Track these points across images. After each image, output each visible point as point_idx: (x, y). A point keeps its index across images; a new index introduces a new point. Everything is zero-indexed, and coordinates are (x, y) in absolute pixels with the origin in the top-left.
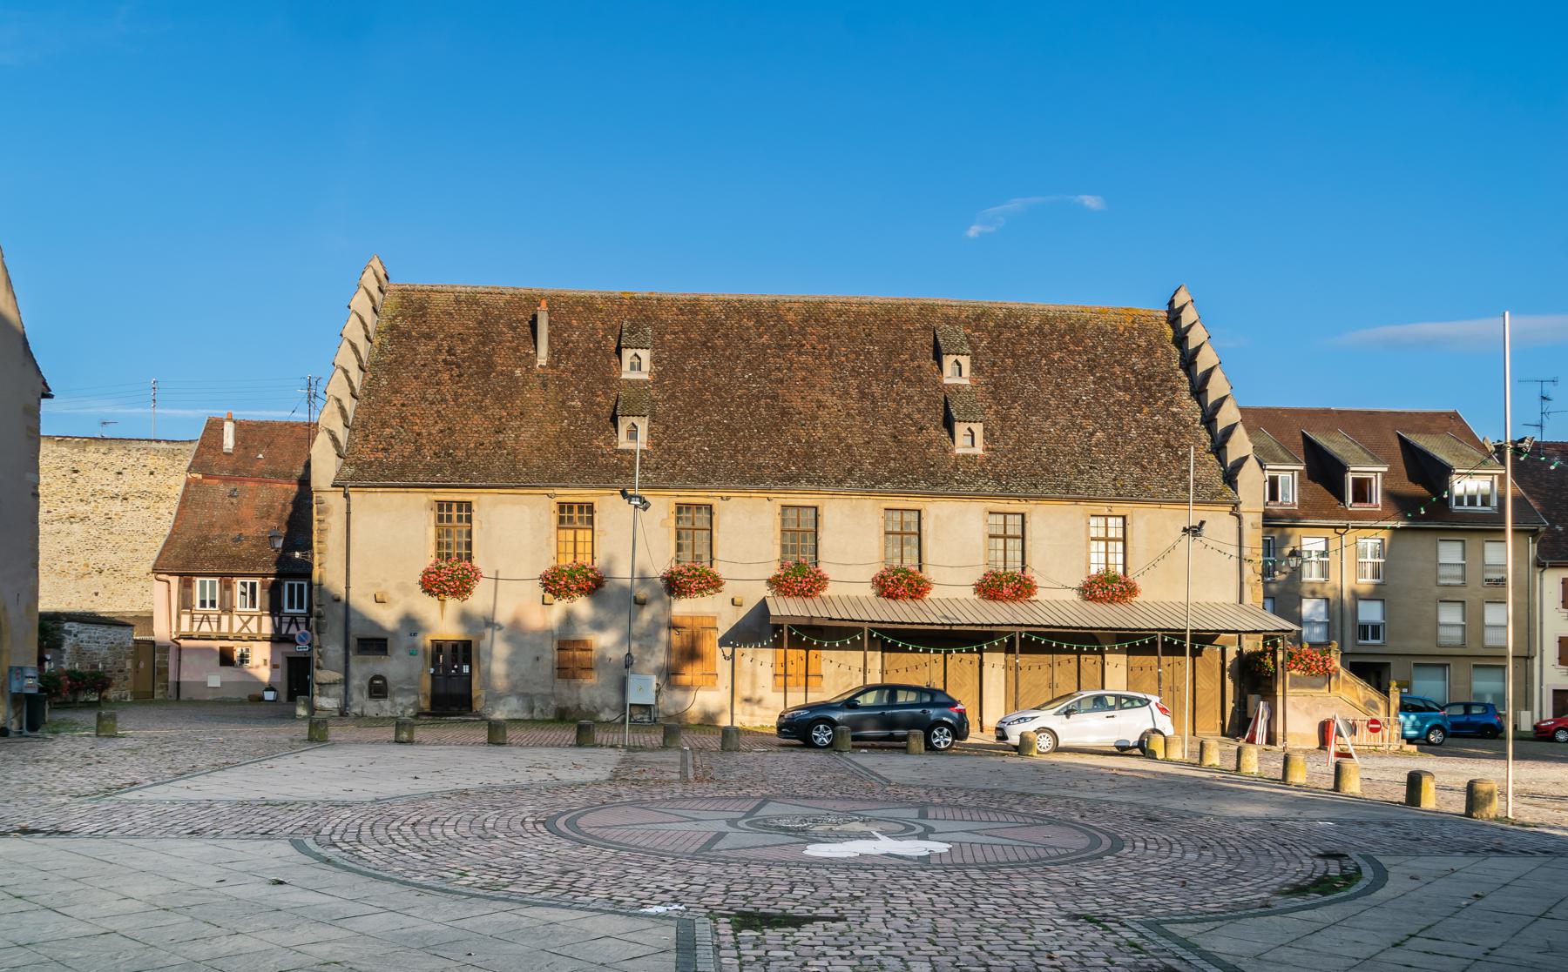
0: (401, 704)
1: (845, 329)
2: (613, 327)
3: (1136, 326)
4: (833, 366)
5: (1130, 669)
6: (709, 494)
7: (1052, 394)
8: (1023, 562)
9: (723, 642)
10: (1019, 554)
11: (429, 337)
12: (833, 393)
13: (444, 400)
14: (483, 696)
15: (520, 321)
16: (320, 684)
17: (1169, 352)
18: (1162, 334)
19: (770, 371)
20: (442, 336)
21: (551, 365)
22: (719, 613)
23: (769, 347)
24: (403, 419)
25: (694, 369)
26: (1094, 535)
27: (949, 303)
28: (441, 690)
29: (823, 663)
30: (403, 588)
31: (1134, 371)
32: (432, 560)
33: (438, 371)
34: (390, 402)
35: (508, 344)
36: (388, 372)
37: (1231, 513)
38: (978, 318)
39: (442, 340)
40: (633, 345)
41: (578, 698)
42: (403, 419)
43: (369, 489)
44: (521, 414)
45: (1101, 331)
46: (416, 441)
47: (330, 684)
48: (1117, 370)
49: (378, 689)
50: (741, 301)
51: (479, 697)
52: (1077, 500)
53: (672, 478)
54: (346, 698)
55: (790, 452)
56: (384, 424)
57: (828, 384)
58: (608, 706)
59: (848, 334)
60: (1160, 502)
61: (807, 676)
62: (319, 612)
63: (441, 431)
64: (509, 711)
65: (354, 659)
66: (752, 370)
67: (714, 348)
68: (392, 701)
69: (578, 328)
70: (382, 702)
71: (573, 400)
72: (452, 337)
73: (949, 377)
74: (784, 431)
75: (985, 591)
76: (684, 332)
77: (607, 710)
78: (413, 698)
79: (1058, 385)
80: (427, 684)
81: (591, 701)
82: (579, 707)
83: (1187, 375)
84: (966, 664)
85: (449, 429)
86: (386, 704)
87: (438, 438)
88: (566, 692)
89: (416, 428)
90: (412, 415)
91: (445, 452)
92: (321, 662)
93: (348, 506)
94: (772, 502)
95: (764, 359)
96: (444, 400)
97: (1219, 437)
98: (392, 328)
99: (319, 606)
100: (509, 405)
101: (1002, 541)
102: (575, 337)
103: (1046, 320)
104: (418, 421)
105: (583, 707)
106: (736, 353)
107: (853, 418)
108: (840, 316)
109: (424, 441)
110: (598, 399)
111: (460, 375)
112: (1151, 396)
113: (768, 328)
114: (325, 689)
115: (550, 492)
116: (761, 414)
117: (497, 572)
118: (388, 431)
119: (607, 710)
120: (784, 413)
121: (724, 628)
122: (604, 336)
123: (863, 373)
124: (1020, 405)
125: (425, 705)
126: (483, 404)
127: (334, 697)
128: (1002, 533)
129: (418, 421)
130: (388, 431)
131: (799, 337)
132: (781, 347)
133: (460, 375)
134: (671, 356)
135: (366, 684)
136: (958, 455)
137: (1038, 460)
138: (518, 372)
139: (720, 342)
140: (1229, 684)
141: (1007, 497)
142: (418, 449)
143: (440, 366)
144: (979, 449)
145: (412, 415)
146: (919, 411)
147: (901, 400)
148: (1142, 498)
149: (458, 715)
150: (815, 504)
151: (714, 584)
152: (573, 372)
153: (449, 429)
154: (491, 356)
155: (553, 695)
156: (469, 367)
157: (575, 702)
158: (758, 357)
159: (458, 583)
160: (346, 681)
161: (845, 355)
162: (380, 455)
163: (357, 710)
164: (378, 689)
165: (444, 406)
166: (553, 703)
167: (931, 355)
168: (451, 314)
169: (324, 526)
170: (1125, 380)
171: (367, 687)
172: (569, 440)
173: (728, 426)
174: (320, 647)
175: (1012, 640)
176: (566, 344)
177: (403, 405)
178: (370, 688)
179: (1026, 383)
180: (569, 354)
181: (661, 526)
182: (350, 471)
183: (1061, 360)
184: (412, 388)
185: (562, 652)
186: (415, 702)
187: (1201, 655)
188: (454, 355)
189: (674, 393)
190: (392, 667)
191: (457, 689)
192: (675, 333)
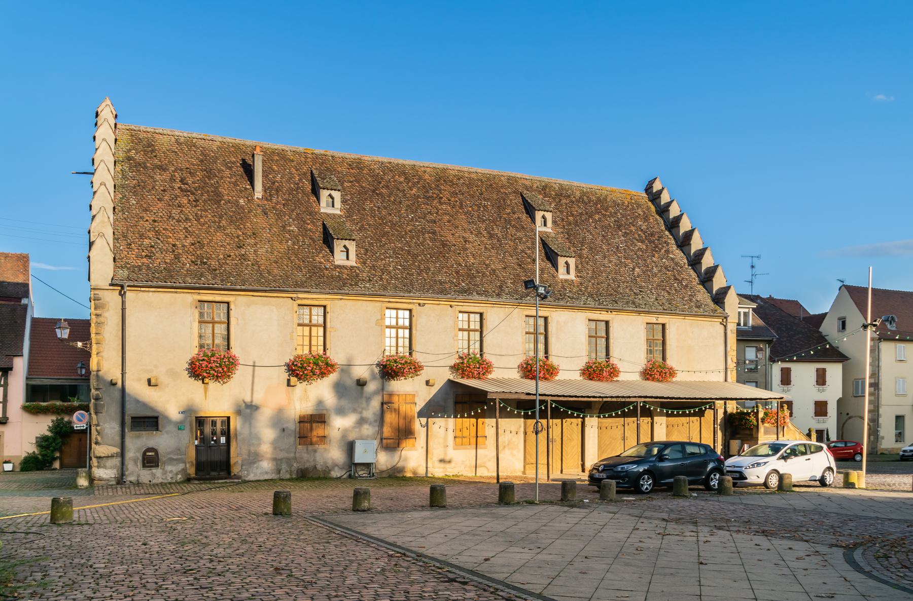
0: (171, 472)
1: (465, 189)
2: (305, 174)
3: (633, 201)
4: (466, 214)
5: (600, 428)
6: (411, 301)
7: (602, 241)
8: (481, 350)
9: (421, 414)
10: (478, 345)
11: (162, 168)
12: (472, 233)
13: (187, 219)
14: (240, 462)
15: (233, 163)
16: (99, 458)
17: (656, 220)
18: (648, 208)
19: (425, 215)
20: (173, 169)
21: (264, 198)
22: (417, 392)
23: (418, 197)
24: (157, 233)
25: (371, 209)
26: (387, 323)
27: (524, 177)
28: (203, 458)
29: (487, 427)
30: (172, 373)
31: (642, 230)
32: (196, 351)
33: (177, 197)
34: (142, 218)
35: (228, 179)
36: (135, 193)
37: (721, 323)
38: (545, 188)
39: (173, 172)
40: (329, 186)
41: (314, 460)
42: (157, 233)
43: (142, 289)
44: (254, 234)
45: (616, 204)
46: (174, 251)
47: (108, 457)
48: (633, 228)
49: (151, 460)
50: (390, 163)
51: (236, 463)
52: (639, 313)
53: (385, 288)
54: (122, 469)
55: (457, 272)
56: (142, 236)
57: (466, 226)
58: (337, 465)
59: (468, 192)
60: (685, 315)
61: (477, 437)
62: (97, 395)
63: (193, 244)
64: (261, 473)
65: (129, 435)
66: (413, 213)
67: (381, 194)
68: (163, 469)
69: (279, 172)
70: (154, 470)
71: (290, 226)
72: (181, 170)
73: (324, 208)
74: (448, 257)
75: (193, 369)
76: (356, 181)
77: (336, 468)
78: (181, 466)
79: (603, 236)
80: (193, 453)
81: (324, 462)
82: (315, 467)
83: (672, 234)
84: (574, 425)
85: (199, 242)
86: (158, 472)
87: (191, 250)
88: (305, 456)
89: (170, 240)
90: (164, 229)
91: (200, 261)
92: (99, 439)
93: (123, 303)
94: (454, 308)
95: (419, 206)
96: (187, 219)
97: (703, 275)
98: (129, 159)
99: (97, 389)
100: (242, 226)
101: (308, 328)
102: (278, 178)
103: (584, 194)
104: (171, 235)
105: (319, 467)
106: (398, 200)
107: (489, 250)
108: (459, 179)
109: (181, 251)
110: (309, 226)
111: (196, 201)
112: (656, 247)
113: (414, 184)
114: (103, 462)
115: (294, 296)
116: (429, 245)
117: (254, 363)
118: (146, 242)
119: (336, 468)
120: (444, 245)
121: (421, 404)
122: (300, 180)
123: (486, 220)
124: (586, 248)
125: (192, 471)
126: (221, 224)
127: (111, 468)
128: (467, 327)
129: (171, 235)
130: (146, 242)
131: (437, 192)
132: (428, 198)
133: (196, 201)
134: (352, 198)
135: (140, 456)
136: (562, 280)
137: (609, 285)
138: (242, 201)
139: (384, 191)
140: (720, 434)
141: (601, 309)
142: (177, 257)
143: (177, 192)
144: (572, 276)
145: (164, 229)
146: (529, 248)
147: (515, 240)
148: (678, 312)
149: (225, 479)
150: (481, 311)
151: (416, 368)
152: (284, 205)
153: (199, 242)
154: (217, 188)
155: (295, 458)
156: (202, 195)
157: (312, 464)
158: (414, 203)
159: (225, 369)
160: (122, 454)
161: (470, 207)
162: (145, 260)
163: (133, 478)
164: (151, 460)
165: (190, 224)
166: (295, 465)
167: (524, 211)
168: (176, 152)
169: (101, 319)
170: (639, 235)
171: (141, 458)
172: (296, 256)
173: (409, 252)
174: (98, 425)
175: (635, 407)
176: (274, 183)
177: (155, 221)
178: (144, 459)
179: (585, 234)
180: (277, 191)
181: (376, 325)
182: (124, 273)
183: (600, 220)
184: (159, 208)
185: (302, 424)
186: (183, 469)
187: (704, 416)
188: (187, 184)
189: (363, 225)
190: (162, 441)
191: (217, 457)
192: (351, 182)
